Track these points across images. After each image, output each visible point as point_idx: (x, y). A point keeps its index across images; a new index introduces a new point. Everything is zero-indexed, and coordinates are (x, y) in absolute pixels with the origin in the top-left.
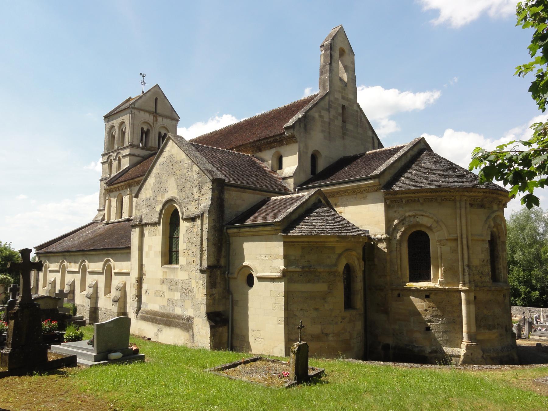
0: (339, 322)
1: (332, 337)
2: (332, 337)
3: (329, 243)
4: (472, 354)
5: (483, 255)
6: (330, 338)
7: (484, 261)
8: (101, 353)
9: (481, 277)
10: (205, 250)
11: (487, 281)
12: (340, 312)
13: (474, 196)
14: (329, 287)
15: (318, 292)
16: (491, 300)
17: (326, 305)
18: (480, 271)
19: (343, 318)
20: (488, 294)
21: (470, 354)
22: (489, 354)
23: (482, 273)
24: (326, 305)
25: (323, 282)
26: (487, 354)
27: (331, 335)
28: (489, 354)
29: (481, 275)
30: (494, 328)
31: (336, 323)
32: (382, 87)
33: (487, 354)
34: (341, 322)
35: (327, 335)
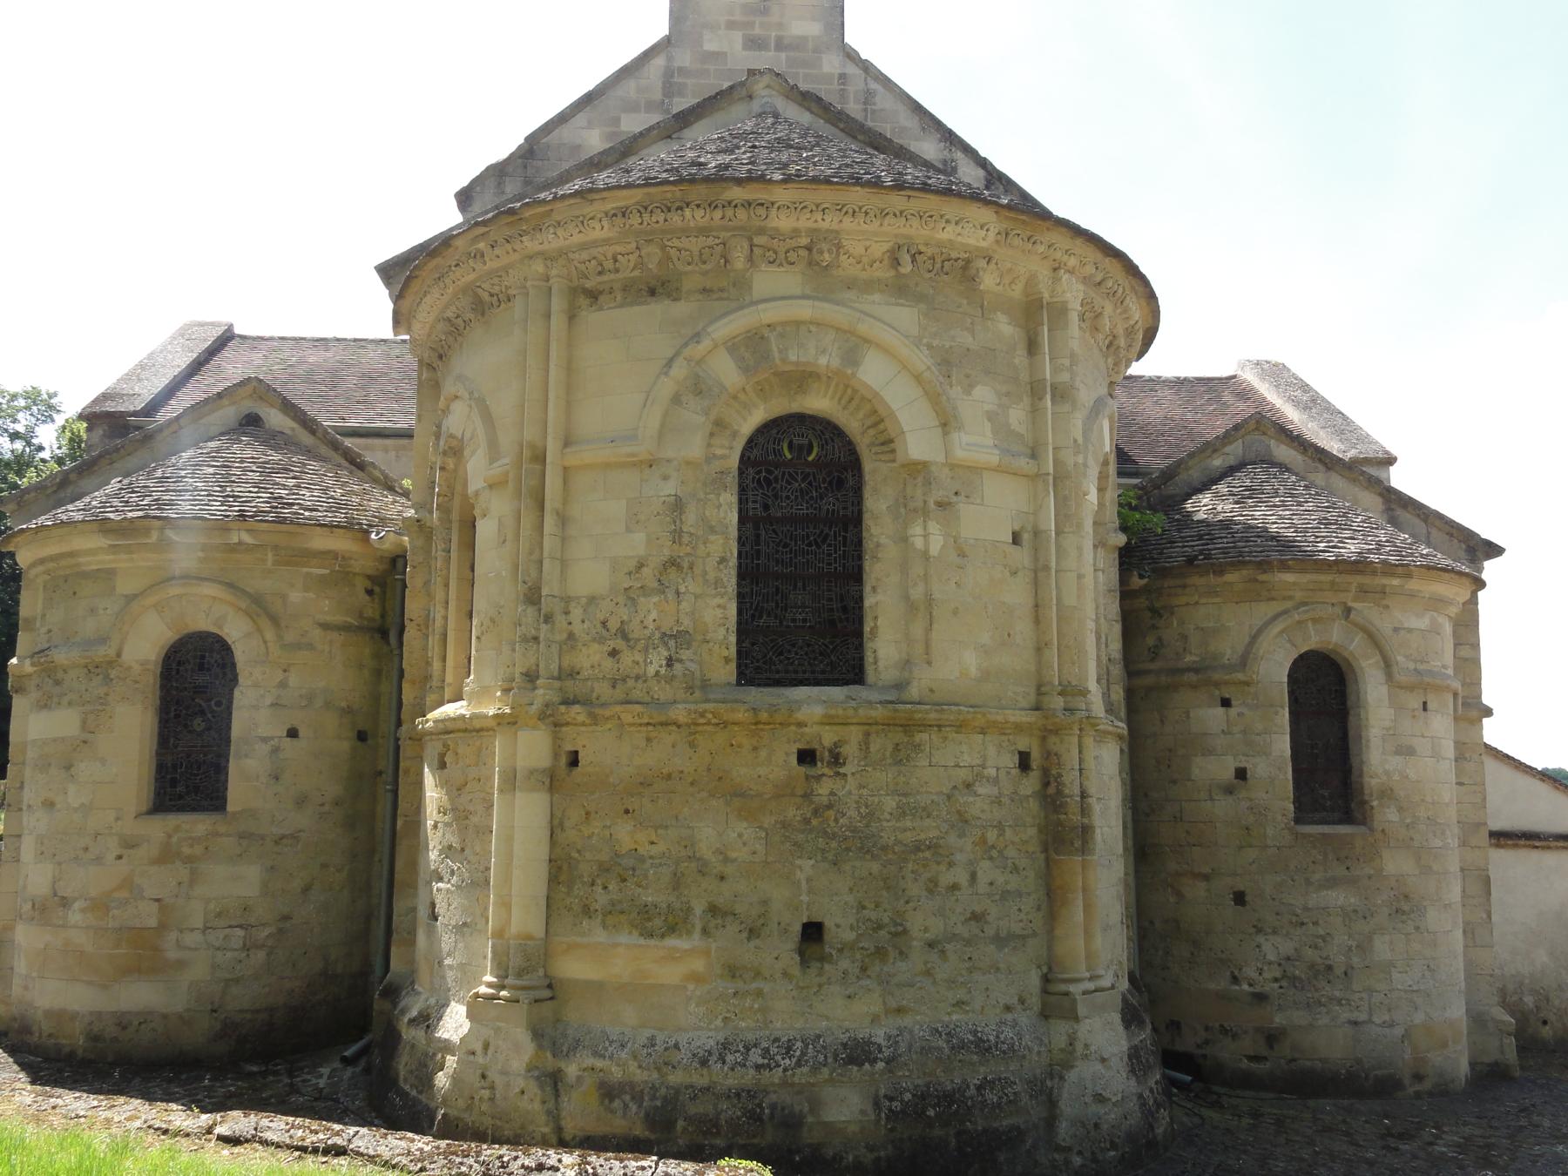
0: (111, 856)
1: (83, 911)
2: (83, 911)
3: (89, 559)
4: (486, 1046)
5: (639, 538)
6: (75, 917)
7: (641, 566)
8: (557, 1091)
9: (614, 653)
10: (435, 827)
11: (651, 670)
12: (117, 819)
13: (584, 247)
14: (84, 722)
15: (55, 740)
16: (669, 777)
17: (72, 788)
18: (614, 625)
19: (129, 844)
20: (649, 740)
21: (478, 1047)
22: (599, 1064)
23: (623, 633)
24: (72, 788)
25: (70, 704)
26: (590, 1061)
27: (77, 905)
28: (599, 1064)
29: (619, 644)
30: (674, 926)
31: (99, 860)
32: (527, 139)
33: (590, 1061)
34: (120, 857)
35: (65, 903)
